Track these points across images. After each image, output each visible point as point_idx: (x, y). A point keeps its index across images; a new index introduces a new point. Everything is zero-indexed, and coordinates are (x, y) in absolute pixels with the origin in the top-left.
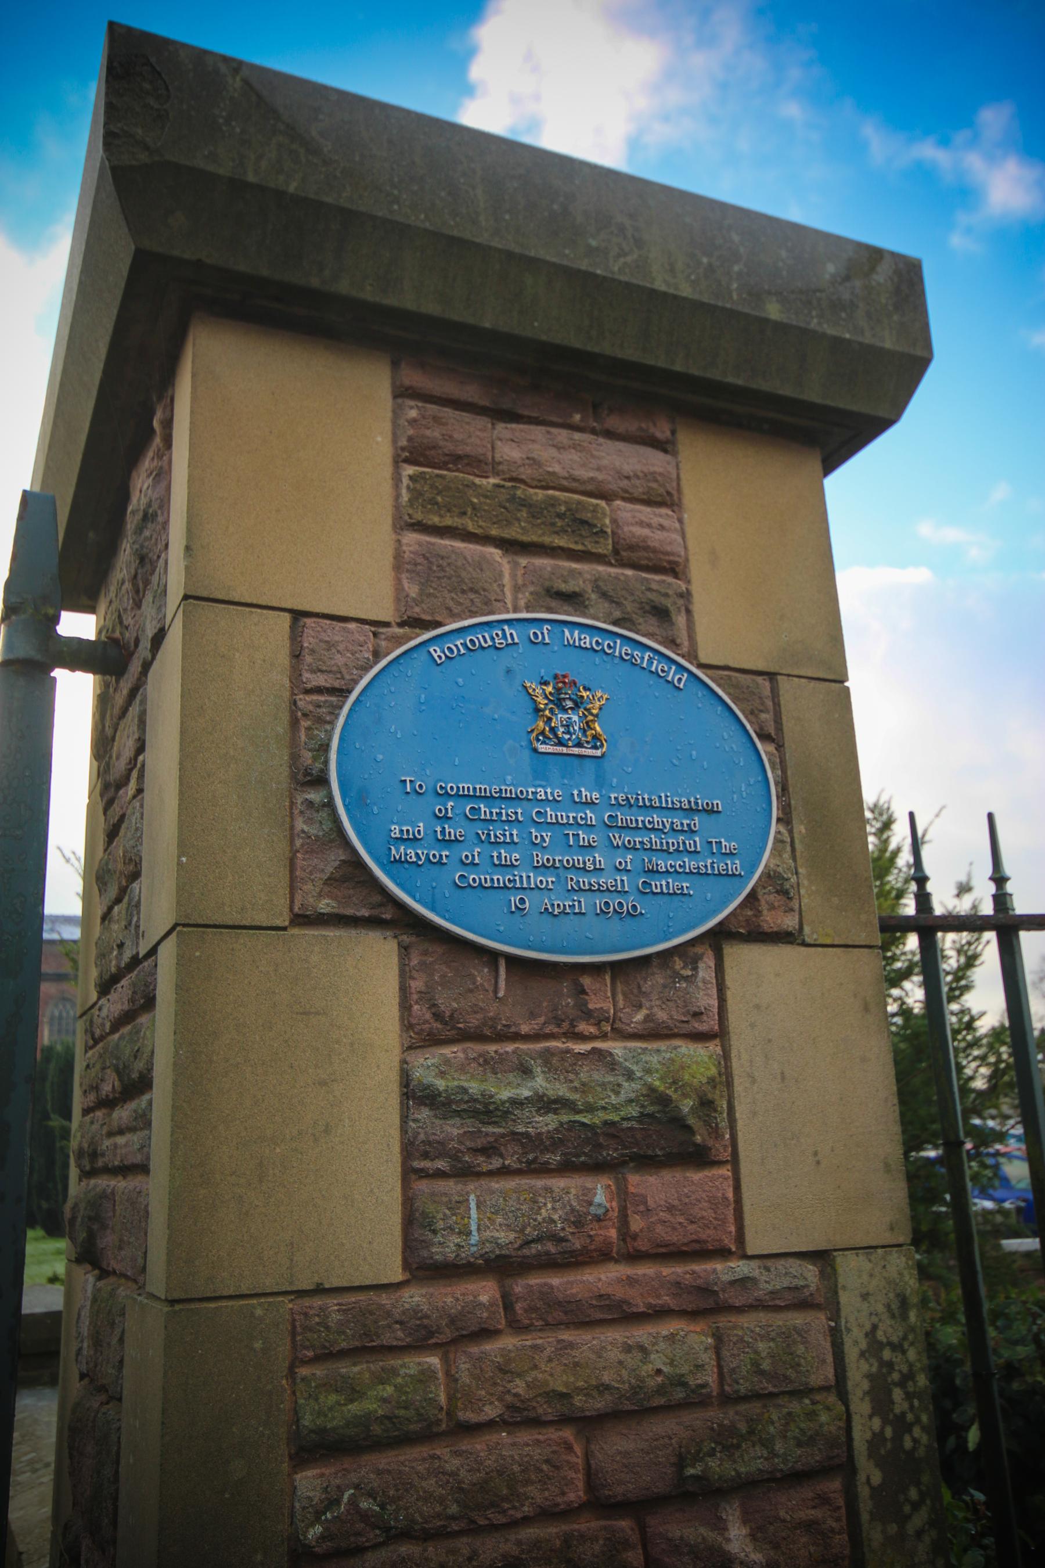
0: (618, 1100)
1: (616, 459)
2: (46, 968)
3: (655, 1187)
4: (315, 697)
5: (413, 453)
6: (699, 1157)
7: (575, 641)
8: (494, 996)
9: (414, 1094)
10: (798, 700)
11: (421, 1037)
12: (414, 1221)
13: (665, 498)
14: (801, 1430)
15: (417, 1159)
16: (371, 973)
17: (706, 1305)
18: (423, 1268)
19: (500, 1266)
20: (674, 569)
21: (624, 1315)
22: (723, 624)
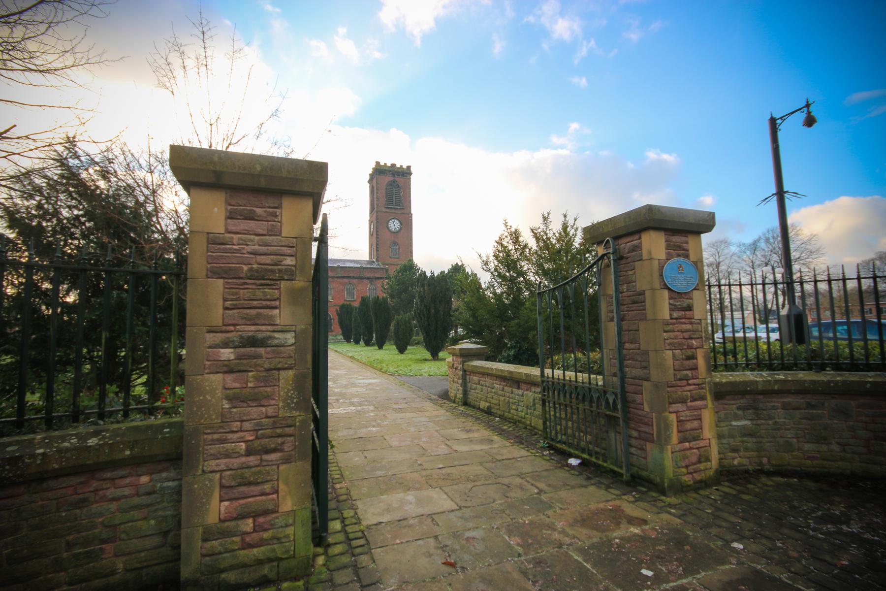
0: (685, 305)
1: (683, 239)
2: (224, 149)
3: (688, 313)
4: (661, 268)
5: (666, 241)
6: (691, 310)
7: (681, 259)
8: (675, 295)
9: (670, 304)
10: (699, 264)
11: (670, 299)
12: (671, 315)
13: (687, 243)
14: (725, 357)
15: (671, 310)
16: (666, 293)
17: (691, 323)
18: (671, 318)
19: (676, 319)
20: (687, 250)
21: (685, 323)
22: (693, 257)
